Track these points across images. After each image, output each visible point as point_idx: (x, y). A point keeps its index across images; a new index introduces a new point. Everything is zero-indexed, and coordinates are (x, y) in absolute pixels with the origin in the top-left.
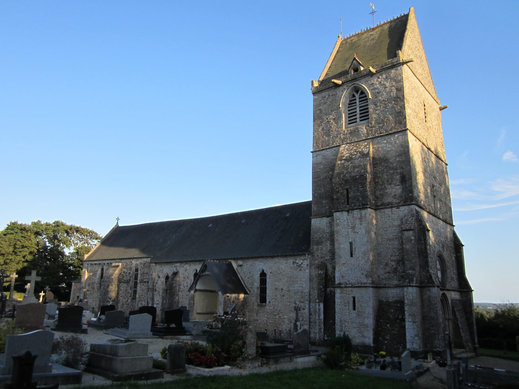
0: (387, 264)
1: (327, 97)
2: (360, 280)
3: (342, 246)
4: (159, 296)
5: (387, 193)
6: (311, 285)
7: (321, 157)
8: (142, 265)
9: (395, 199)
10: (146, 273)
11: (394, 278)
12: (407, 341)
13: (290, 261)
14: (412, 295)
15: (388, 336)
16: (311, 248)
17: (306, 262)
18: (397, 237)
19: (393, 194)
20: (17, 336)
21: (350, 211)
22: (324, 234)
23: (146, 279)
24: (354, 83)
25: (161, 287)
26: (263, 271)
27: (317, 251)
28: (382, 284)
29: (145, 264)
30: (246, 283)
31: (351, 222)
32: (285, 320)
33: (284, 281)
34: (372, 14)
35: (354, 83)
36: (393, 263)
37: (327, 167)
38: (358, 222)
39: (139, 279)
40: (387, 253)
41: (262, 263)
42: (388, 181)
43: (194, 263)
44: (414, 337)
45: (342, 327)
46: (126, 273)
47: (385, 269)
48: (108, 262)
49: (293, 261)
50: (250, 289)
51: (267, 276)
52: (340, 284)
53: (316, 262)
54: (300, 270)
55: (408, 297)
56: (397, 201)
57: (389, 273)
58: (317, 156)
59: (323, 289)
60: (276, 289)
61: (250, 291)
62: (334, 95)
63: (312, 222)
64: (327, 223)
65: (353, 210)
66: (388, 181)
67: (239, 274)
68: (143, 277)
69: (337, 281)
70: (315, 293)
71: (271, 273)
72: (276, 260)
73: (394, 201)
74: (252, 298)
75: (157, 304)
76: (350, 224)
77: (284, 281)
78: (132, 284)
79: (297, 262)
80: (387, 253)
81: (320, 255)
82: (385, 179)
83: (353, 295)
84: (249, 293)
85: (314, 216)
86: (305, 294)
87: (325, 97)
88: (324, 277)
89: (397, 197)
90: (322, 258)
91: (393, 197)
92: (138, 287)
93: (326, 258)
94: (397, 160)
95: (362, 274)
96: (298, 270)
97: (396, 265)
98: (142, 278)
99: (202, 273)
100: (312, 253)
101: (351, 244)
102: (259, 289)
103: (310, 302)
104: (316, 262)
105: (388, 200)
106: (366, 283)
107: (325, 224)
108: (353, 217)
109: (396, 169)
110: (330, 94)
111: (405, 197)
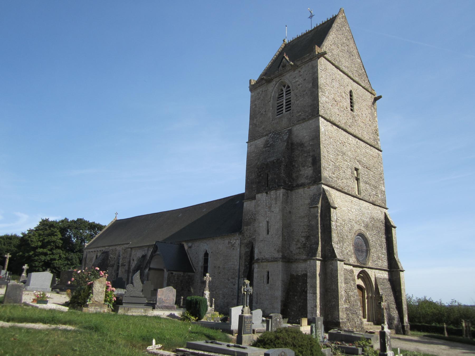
0: (298, 241)
1: (261, 93)
2: (273, 255)
3: (261, 225)
5: (301, 174)
6: (241, 262)
7: (254, 146)
8: (123, 251)
9: (307, 179)
11: (303, 253)
12: (308, 312)
14: (314, 268)
15: (294, 308)
16: (242, 229)
17: (238, 242)
18: (307, 214)
19: (306, 175)
21: (268, 193)
22: (252, 215)
24: (281, 78)
26: (206, 251)
27: (247, 231)
28: (294, 259)
29: (125, 249)
30: (193, 263)
31: (268, 203)
32: (220, 295)
34: (310, 18)
35: (281, 78)
36: (303, 239)
37: (257, 155)
38: (273, 202)
39: (120, 264)
40: (299, 230)
41: (205, 244)
42: (302, 163)
44: (313, 308)
45: (258, 300)
46: (112, 258)
47: (297, 245)
48: (100, 249)
49: (229, 241)
50: (196, 268)
51: (209, 256)
52: (258, 259)
53: (245, 241)
54: (233, 249)
55: (310, 270)
56: (309, 182)
57: (299, 248)
58: (250, 146)
59: (248, 266)
60: (215, 267)
61: (196, 270)
62: (266, 90)
63: (245, 205)
66: (302, 163)
67: (189, 254)
68: (124, 261)
70: (242, 269)
73: (306, 182)
74: (197, 276)
76: (268, 204)
78: (115, 267)
79: (231, 242)
80: (299, 230)
81: (248, 235)
82: (300, 161)
83: (267, 269)
84: (195, 271)
85: (246, 200)
86: (236, 270)
87: (259, 93)
88: (249, 254)
89: (309, 177)
90: (250, 237)
91: (305, 178)
92: (119, 270)
93: (253, 237)
94: (311, 143)
96: (232, 249)
97: (305, 241)
99: (154, 253)
100: (243, 233)
101: (268, 222)
102: (203, 268)
103: (239, 278)
104: (245, 241)
105: (302, 180)
107: (253, 207)
108: (271, 197)
109: (309, 152)
110: (263, 91)
111: (315, 177)
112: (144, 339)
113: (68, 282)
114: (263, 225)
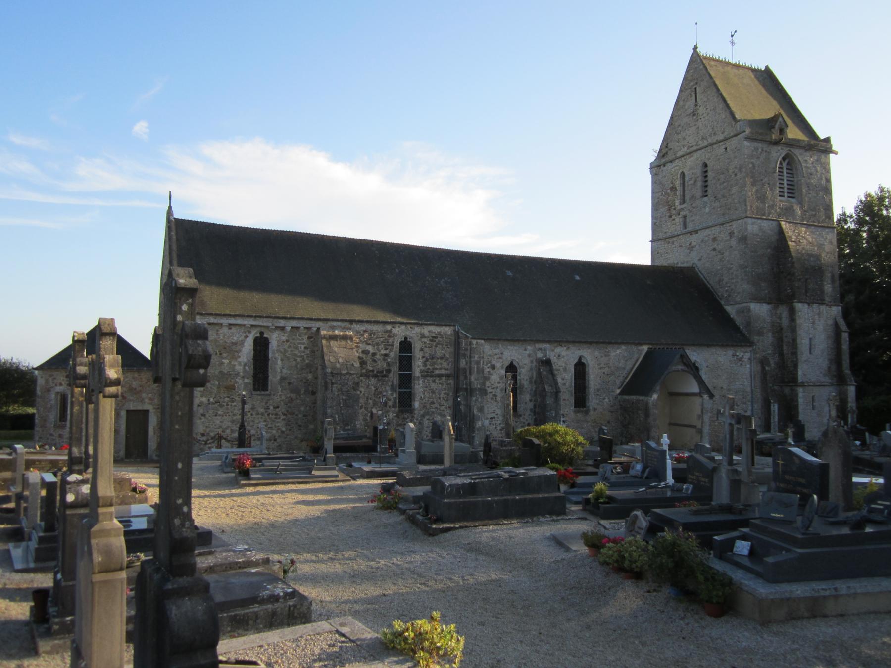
4: (495, 404)
10: (441, 358)
13: (730, 352)
17: (747, 355)
20: (8, 524)
23: (440, 369)
25: (499, 385)
29: (436, 338)
33: (724, 377)
38: (816, 317)
41: (695, 353)
43: (577, 345)
52: (802, 382)
54: (741, 364)
64: (767, 311)
65: (813, 303)
69: (800, 380)
71: (707, 367)
72: (713, 350)
75: (491, 418)
77: (724, 377)
78: (394, 378)
79: (737, 354)
95: (821, 373)
98: (428, 366)
101: (810, 339)
104: (758, 356)
106: (823, 382)
108: (813, 311)
112: (401, 523)
113: (177, 466)
114: (806, 342)
